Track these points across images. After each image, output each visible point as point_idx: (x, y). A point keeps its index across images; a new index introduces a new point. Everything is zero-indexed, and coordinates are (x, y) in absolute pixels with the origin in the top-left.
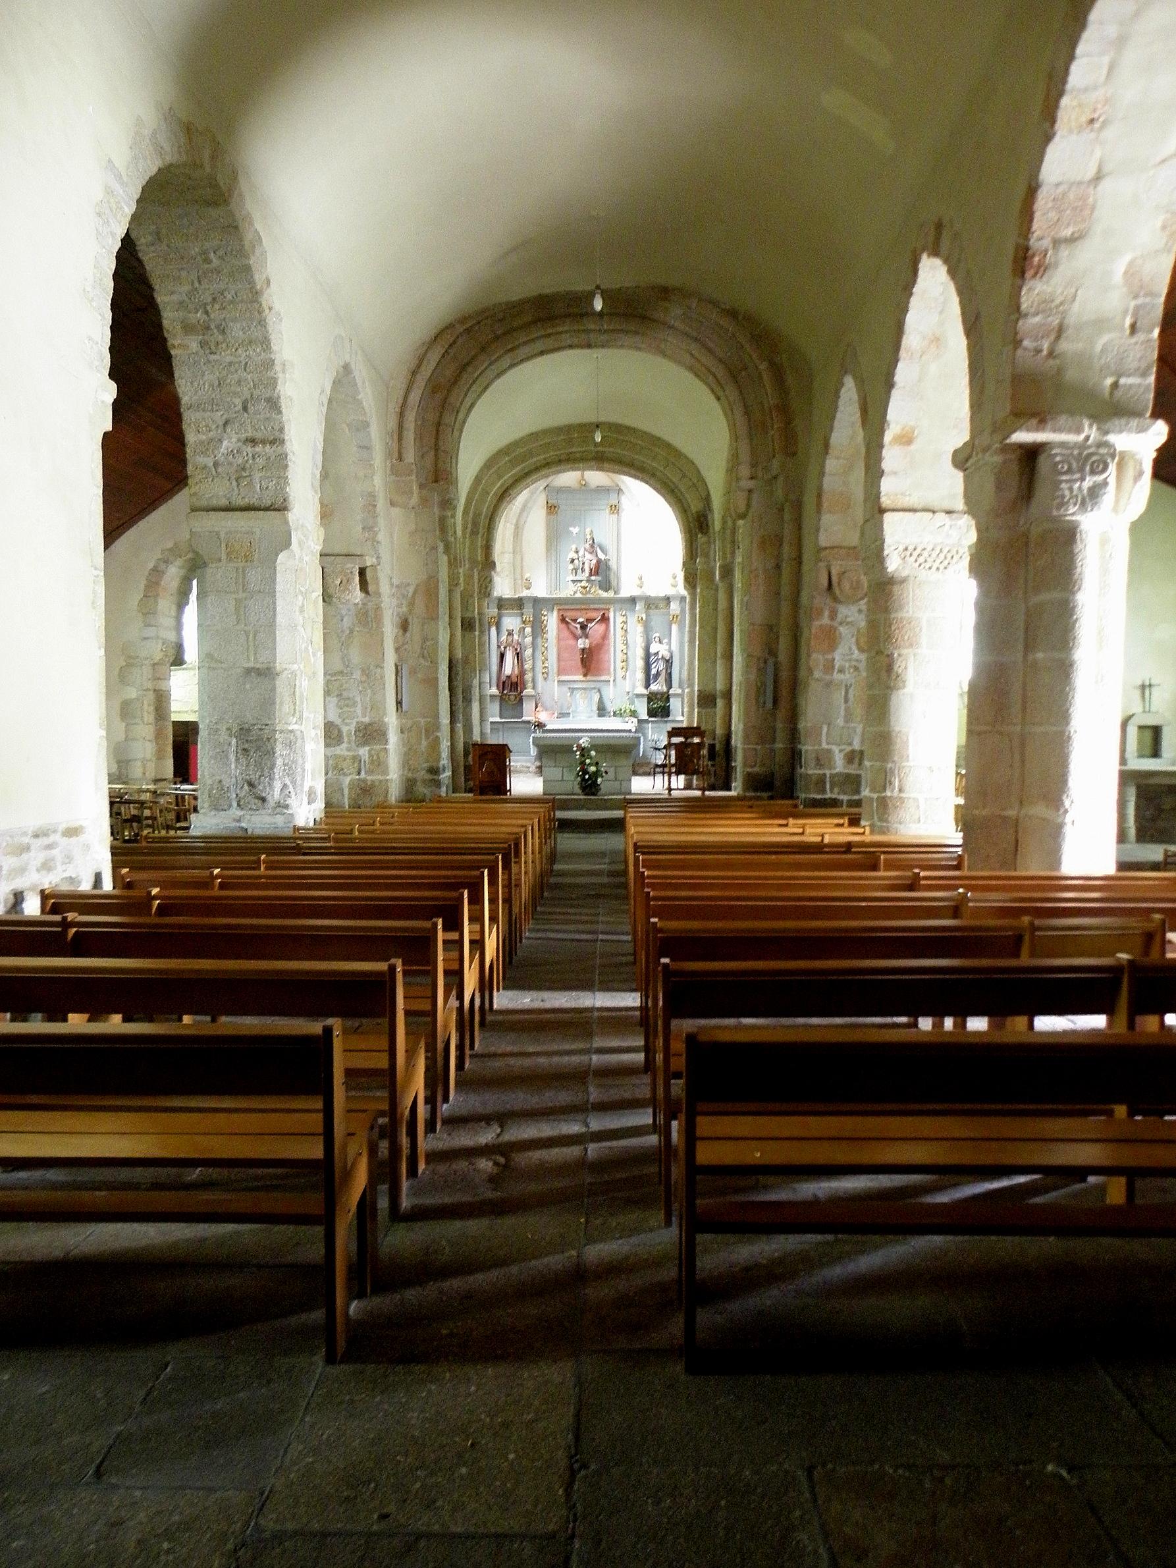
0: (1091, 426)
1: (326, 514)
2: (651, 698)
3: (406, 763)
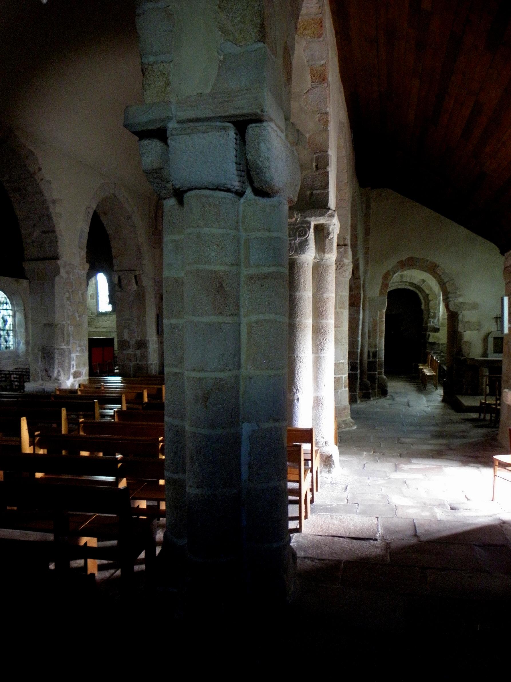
0: (297, 215)
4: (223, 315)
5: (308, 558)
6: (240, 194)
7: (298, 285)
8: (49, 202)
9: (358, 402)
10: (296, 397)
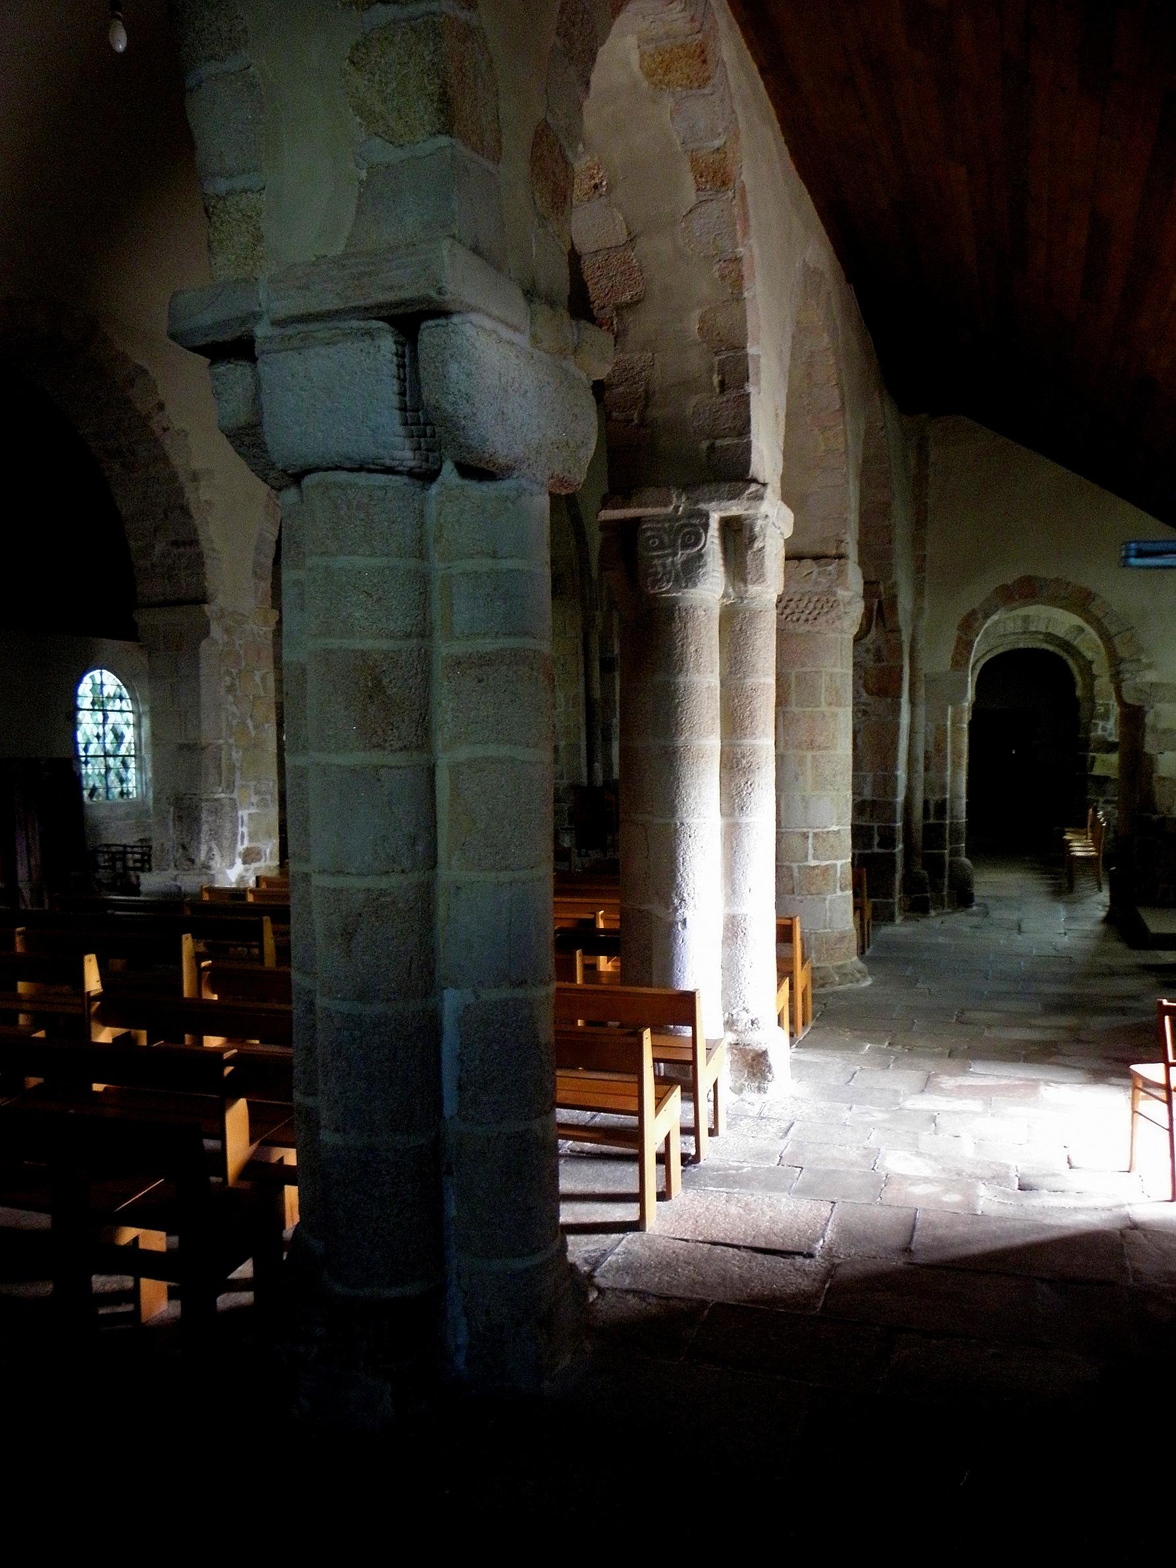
0: (679, 497)
4: (384, 749)
5: (635, 1292)
6: (426, 476)
7: (682, 659)
8: (183, 478)
9: (898, 921)
10: (679, 918)
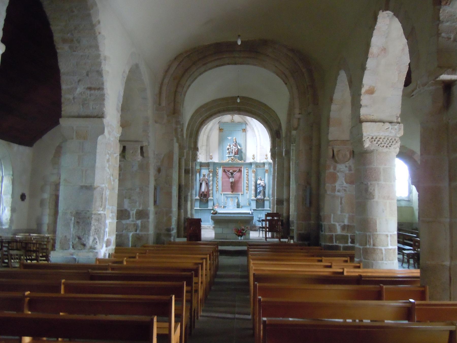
1: (124, 124)
2: (257, 201)
3: (157, 226)
8: (102, 57)
